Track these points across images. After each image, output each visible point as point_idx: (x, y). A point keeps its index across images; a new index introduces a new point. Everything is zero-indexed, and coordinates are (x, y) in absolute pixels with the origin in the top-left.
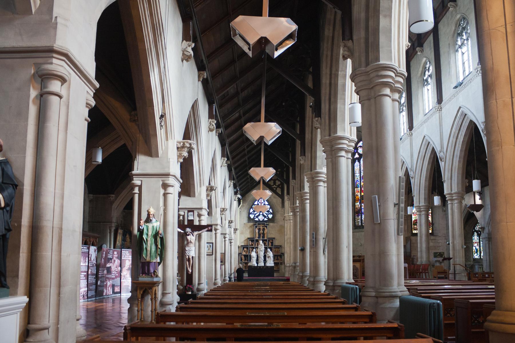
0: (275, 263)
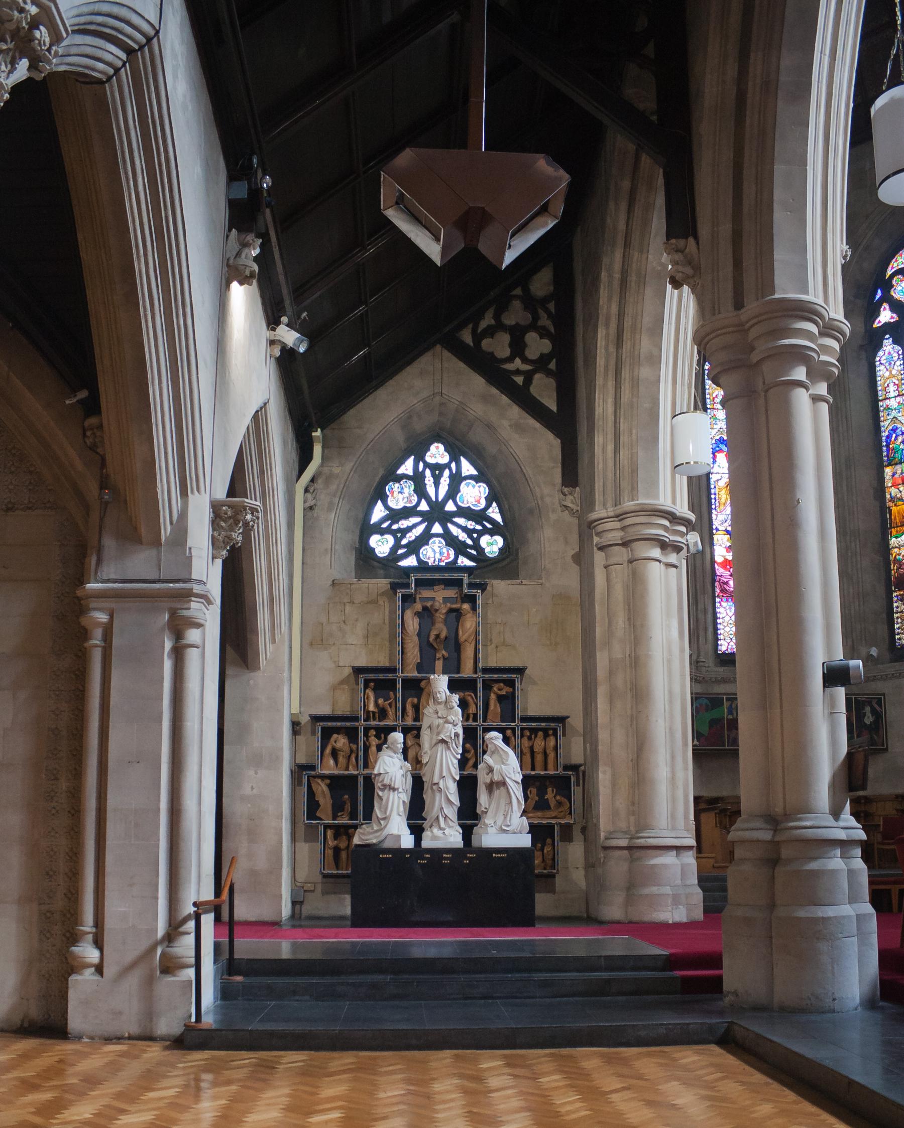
0: (533, 829)
